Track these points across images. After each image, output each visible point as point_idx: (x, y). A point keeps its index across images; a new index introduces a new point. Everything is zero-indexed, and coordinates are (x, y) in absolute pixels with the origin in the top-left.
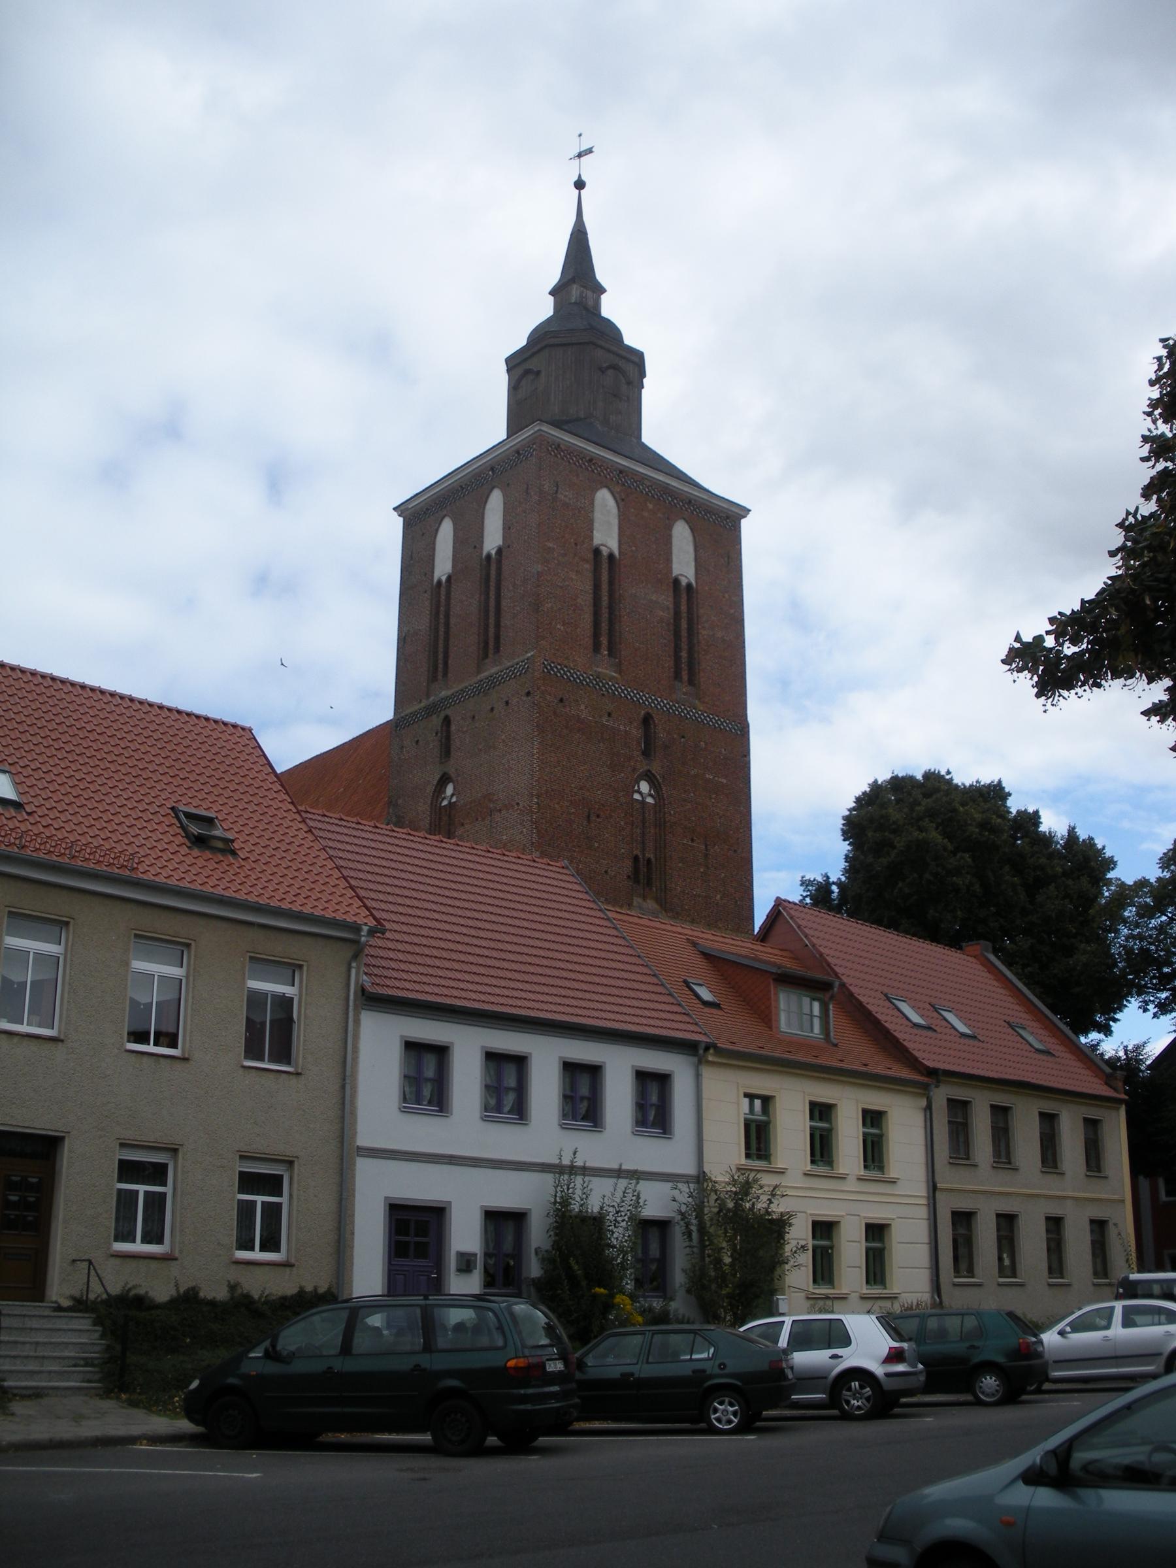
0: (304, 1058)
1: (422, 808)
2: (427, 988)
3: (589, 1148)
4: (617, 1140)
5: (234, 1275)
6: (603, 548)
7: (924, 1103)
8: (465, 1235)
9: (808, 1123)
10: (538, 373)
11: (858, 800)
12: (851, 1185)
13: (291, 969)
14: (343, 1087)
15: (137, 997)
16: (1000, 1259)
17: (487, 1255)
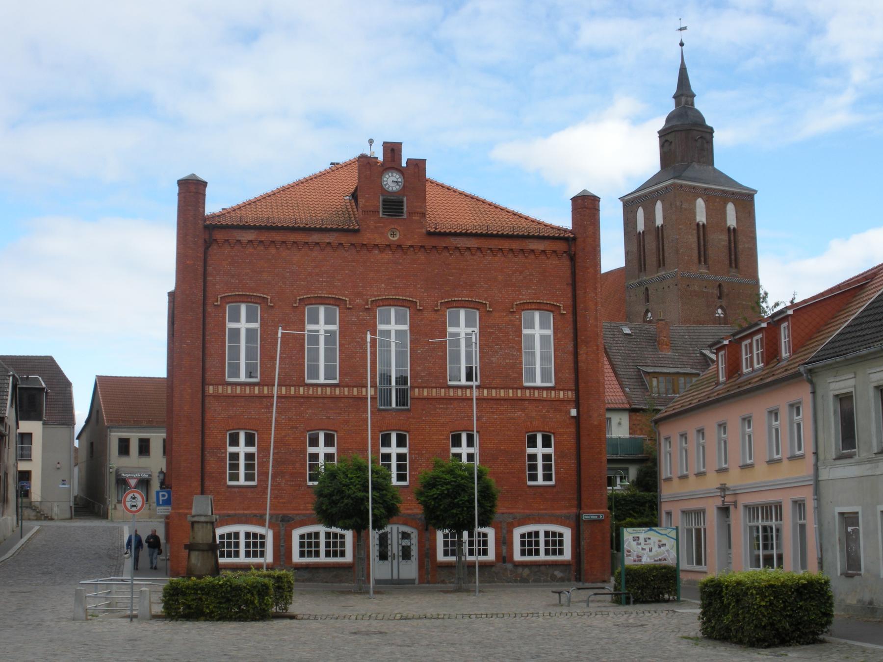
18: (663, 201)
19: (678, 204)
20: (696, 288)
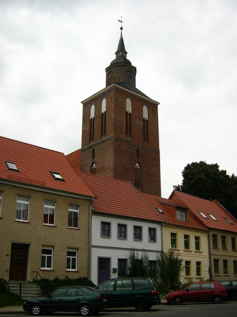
0: (81, 226)
1: (88, 169)
2: (106, 210)
3: (138, 245)
4: (145, 243)
5: (66, 274)
7: (208, 235)
8: (114, 265)
9: (184, 239)
10: (113, 72)
11: (185, 168)
12: (193, 253)
13: (77, 207)
14: (89, 232)
15: (18, 209)
16: (224, 270)
17: (119, 269)
20: (124, 148)
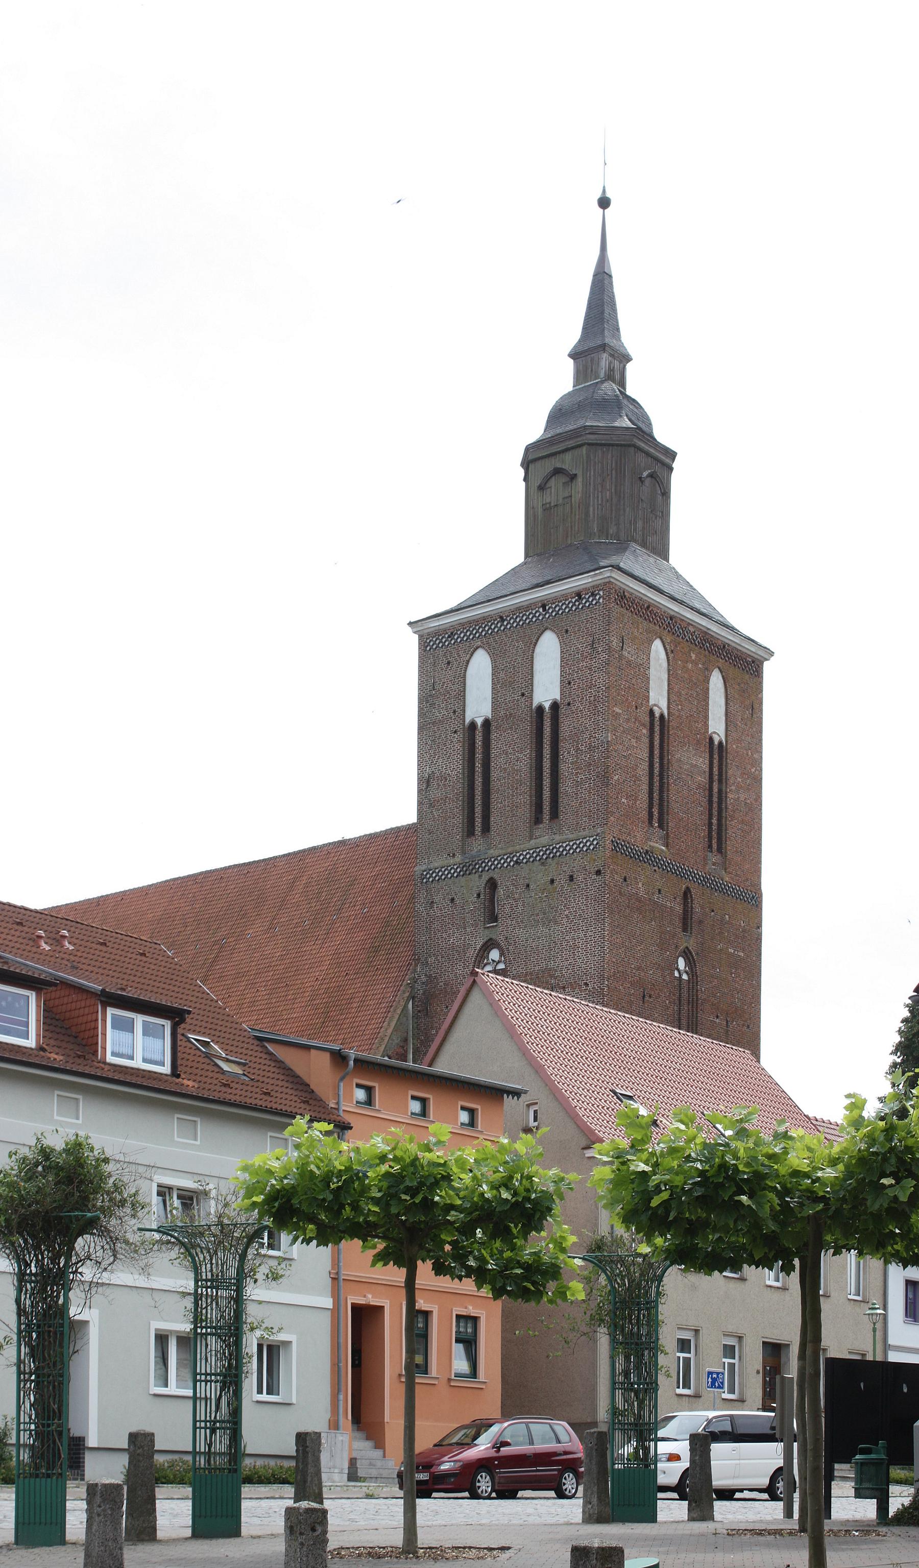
6: (655, 708)
10: (573, 477)
18: (563, 634)
19: (615, 643)
